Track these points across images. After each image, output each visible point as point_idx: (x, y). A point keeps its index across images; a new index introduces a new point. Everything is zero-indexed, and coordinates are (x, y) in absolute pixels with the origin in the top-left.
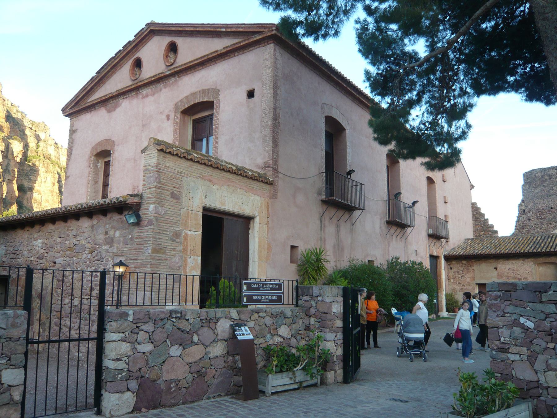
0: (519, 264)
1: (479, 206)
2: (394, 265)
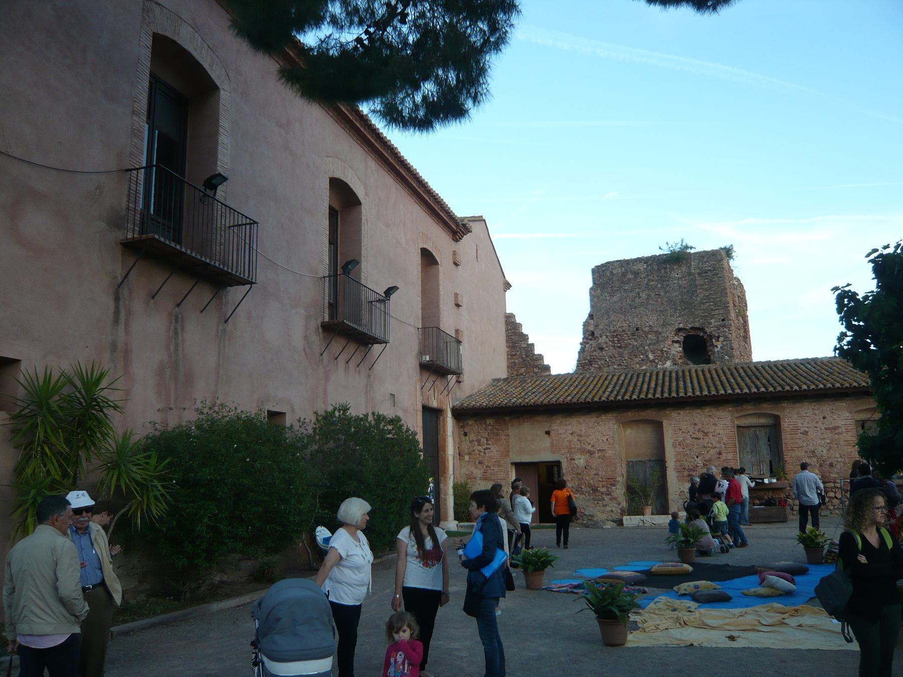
0: (591, 424)
2: (334, 424)
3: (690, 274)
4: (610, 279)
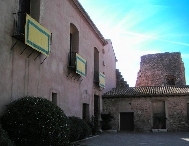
1: (119, 71)
3: (170, 59)
4: (146, 60)
